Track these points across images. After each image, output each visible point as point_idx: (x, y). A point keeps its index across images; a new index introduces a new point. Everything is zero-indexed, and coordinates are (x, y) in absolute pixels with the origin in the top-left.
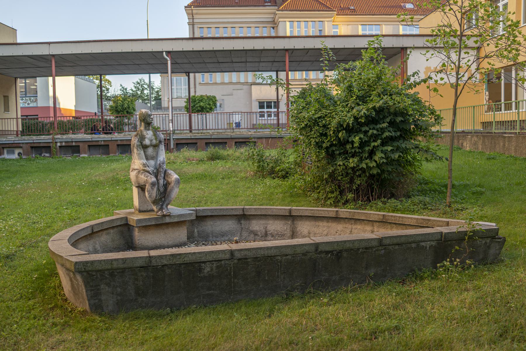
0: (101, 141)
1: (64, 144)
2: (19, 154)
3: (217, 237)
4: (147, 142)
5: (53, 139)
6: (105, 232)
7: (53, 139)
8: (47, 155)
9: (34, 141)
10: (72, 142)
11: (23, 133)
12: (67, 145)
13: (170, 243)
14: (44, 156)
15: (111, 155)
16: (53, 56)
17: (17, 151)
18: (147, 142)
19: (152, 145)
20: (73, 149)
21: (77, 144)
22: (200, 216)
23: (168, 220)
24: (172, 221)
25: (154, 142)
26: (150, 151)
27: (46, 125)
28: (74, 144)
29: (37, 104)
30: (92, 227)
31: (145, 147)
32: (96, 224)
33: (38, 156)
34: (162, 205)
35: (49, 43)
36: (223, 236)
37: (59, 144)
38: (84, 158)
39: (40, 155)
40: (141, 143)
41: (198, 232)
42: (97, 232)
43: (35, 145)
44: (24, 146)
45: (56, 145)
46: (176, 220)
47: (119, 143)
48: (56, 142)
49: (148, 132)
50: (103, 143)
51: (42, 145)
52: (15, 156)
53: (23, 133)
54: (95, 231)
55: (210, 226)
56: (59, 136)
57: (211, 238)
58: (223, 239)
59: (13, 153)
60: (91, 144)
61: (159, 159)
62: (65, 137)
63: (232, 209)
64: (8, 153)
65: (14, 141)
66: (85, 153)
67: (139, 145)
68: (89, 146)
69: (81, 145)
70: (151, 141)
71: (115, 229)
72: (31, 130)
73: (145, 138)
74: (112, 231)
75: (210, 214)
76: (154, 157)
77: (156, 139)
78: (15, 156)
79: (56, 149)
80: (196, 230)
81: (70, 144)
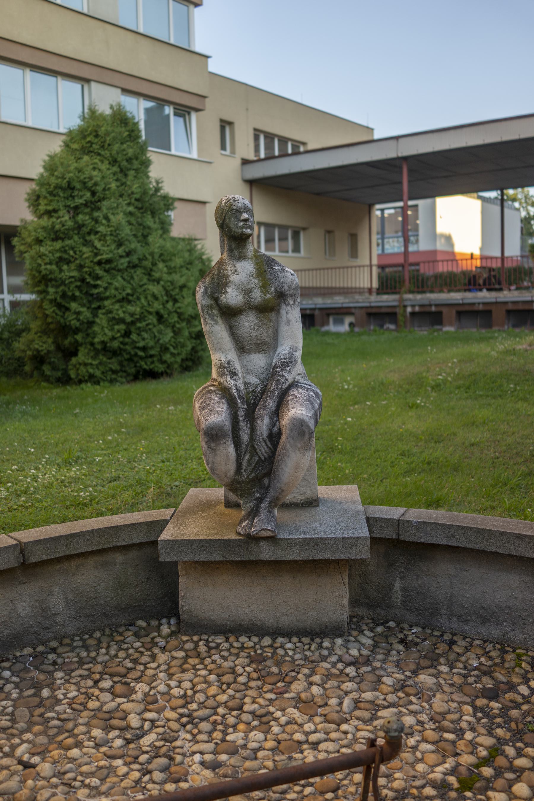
0: (479, 304)
1: (417, 309)
2: (351, 325)
3: (467, 621)
4: (232, 297)
5: (401, 300)
6: (91, 561)
7: (401, 300)
8: (392, 327)
9: (373, 305)
10: (430, 305)
11: (381, 291)
12: (423, 310)
13: (286, 621)
14: (388, 329)
15: (495, 328)
16: (405, 159)
17: (348, 320)
18: (232, 297)
19: (249, 307)
20: (431, 317)
21: (488, 308)
22: (405, 542)
23: (266, 552)
24: (280, 555)
25: (257, 296)
26: (248, 323)
27: (428, 278)
28: (433, 309)
29: (418, 247)
30: (22, 548)
31: (229, 314)
32: (38, 542)
33: (377, 328)
34: (260, 500)
35: (397, 138)
36: (485, 620)
37: (409, 310)
38: (447, 333)
39: (382, 326)
40: (216, 300)
41: (404, 590)
42: (36, 565)
43: (374, 311)
44: (357, 311)
45: (405, 311)
46: (296, 555)
47: (510, 307)
48: (405, 307)
49: (239, 265)
50: (481, 307)
51: (383, 310)
52: (345, 328)
53: (381, 291)
54: (33, 559)
55: (443, 580)
56: (410, 296)
57: (443, 620)
58: (484, 631)
59: (342, 322)
60: (461, 309)
61: (279, 350)
62: (419, 297)
63: (520, 537)
64: (336, 322)
65: (342, 303)
66: (451, 324)
67: (210, 307)
68: (460, 314)
69: (445, 310)
70: (247, 292)
71: (133, 554)
72: (387, 286)
73: (226, 285)
74: (119, 558)
75: (442, 541)
76: (264, 344)
77: (264, 287)
78: (345, 328)
79: (405, 317)
80: (398, 585)
81: (427, 309)
